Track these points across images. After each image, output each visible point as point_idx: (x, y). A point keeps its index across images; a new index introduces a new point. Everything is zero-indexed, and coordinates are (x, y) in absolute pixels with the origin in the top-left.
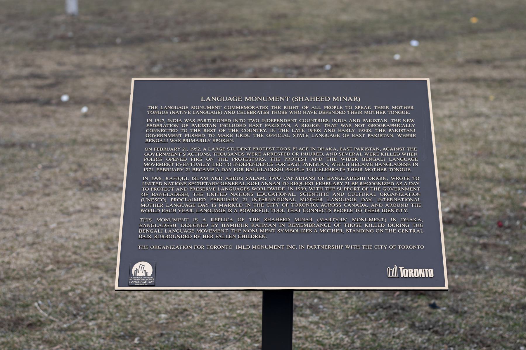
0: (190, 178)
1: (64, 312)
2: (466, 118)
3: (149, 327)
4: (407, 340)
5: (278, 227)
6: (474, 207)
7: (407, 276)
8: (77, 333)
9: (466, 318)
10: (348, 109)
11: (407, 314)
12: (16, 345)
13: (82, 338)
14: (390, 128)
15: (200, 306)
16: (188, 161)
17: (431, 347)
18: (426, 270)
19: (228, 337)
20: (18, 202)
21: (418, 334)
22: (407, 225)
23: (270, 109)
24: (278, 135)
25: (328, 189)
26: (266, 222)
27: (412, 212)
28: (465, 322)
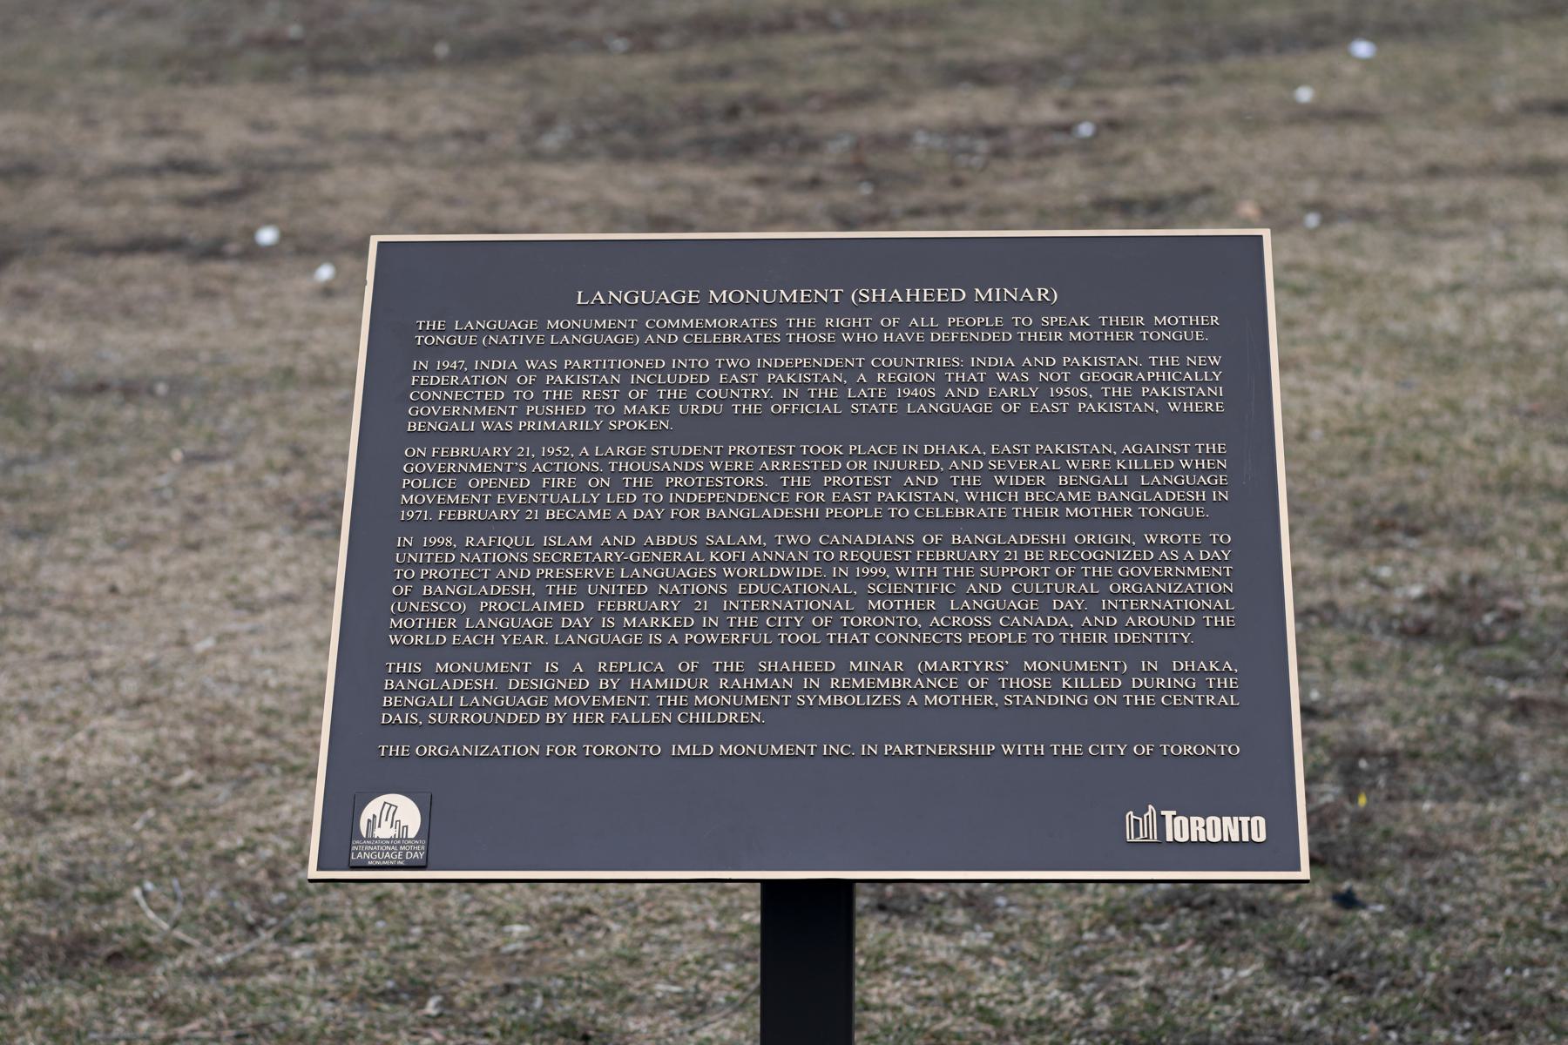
0: (537, 540)
1: (217, 917)
2: (1503, 292)
3: (471, 963)
4: (1255, 1008)
5: (798, 688)
6: (1501, 583)
7: (1185, 839)
8: (254, 983)
9: (1445, 938)
10: (1022, 328)
11: (1264, 924)
12: (69, 1020)
13: (268, 1000)
14: (1146, 383)
15: (631, 899)
16: (535, 488)
17: (1328, 1030)
18: (1245, 820)
19: (709, 995)
20: (102, 571)
21: (1292, 988)
22: (1190, 682)
23: (783, 327)
24: (805, 409)
25: (952, 571)
26: (762, 675)
27: (1206, 641)
28: (1439, 950)
